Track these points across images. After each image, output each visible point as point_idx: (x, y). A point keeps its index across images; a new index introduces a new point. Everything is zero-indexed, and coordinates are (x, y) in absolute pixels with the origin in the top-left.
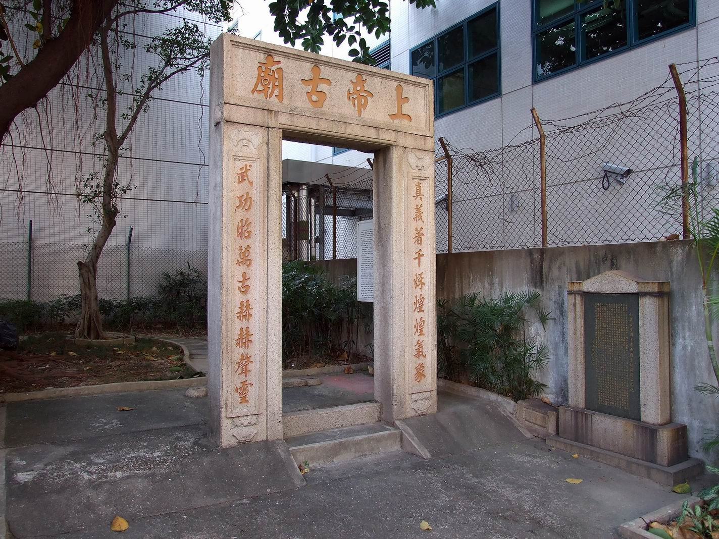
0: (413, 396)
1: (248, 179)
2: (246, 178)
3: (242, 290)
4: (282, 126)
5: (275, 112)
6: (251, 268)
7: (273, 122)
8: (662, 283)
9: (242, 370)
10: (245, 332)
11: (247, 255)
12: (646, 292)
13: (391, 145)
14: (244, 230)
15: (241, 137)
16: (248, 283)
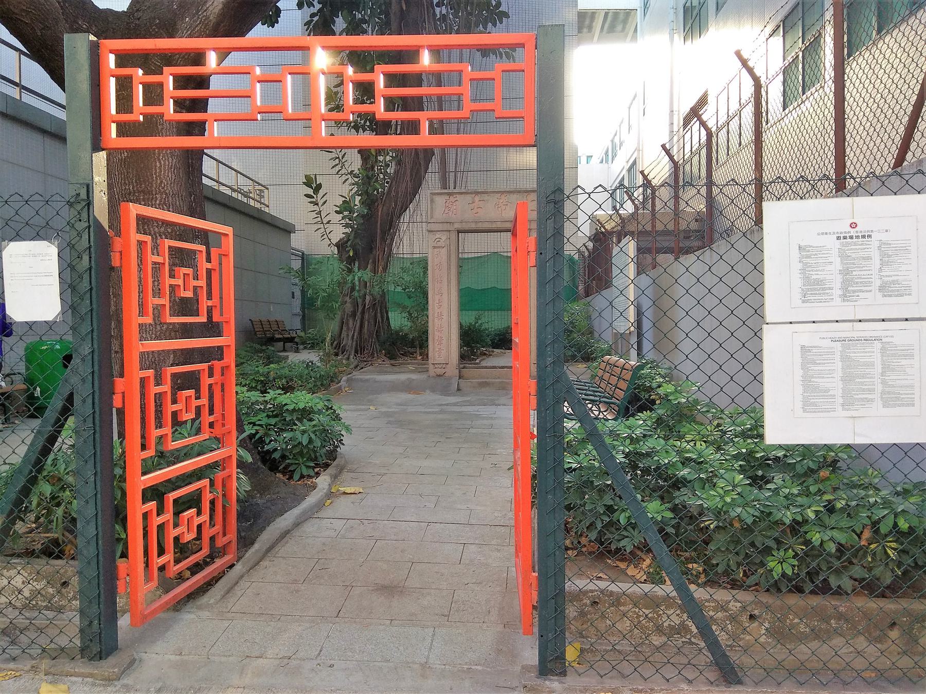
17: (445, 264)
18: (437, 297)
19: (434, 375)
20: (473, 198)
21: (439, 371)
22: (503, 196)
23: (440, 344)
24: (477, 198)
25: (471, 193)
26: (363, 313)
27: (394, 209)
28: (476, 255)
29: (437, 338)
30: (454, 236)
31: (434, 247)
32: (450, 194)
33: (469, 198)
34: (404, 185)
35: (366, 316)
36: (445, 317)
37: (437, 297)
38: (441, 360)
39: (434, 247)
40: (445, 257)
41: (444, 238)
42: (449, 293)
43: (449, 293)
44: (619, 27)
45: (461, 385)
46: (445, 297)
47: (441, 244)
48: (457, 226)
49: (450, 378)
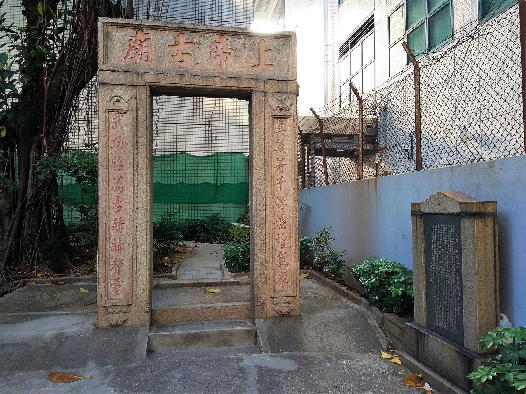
0: (275, 300)
1: (121, 126)
2: (118, 125)
3: (116, 210)
4: (147, 84)
5: (142, 73)
6: (123, 193)
7: (140, 81)
8: (485, 203)
9: (116, 270)
10: (118, 242)
11: (120, 183)
12: (467, 213)
13: (252, 91)
14: (117, 165)
15: (113, 95)
16: (120, 204)
17: (128, 140)
18: (114, 194)
19: (106, 325)
20: (176, 38)
21: (115, 318)
22: (223, 39)
23: (118, 271)
24: (182, 39)
25: (171, 29)
26: (23, 210)
27: (67, 83)
28: (166, 154)
29: (112, 261)
30: (144, 94)
31: (110, 111)
32: (138, 28)
33: (169, 37)
34: (80, 56)
35: (27, 215)
36: (127, 225)
37: (114, 194)
38: (120, 299)
39: (110, 111)
40: (128, 129)
41: (127, 97)
42: (135, 185)
43: (135, 185)
44: (263, 8)
45: (155, 342)
46: (128, 192)
47: (122, 105)
48: (149, 78)
49: (135, 330)
